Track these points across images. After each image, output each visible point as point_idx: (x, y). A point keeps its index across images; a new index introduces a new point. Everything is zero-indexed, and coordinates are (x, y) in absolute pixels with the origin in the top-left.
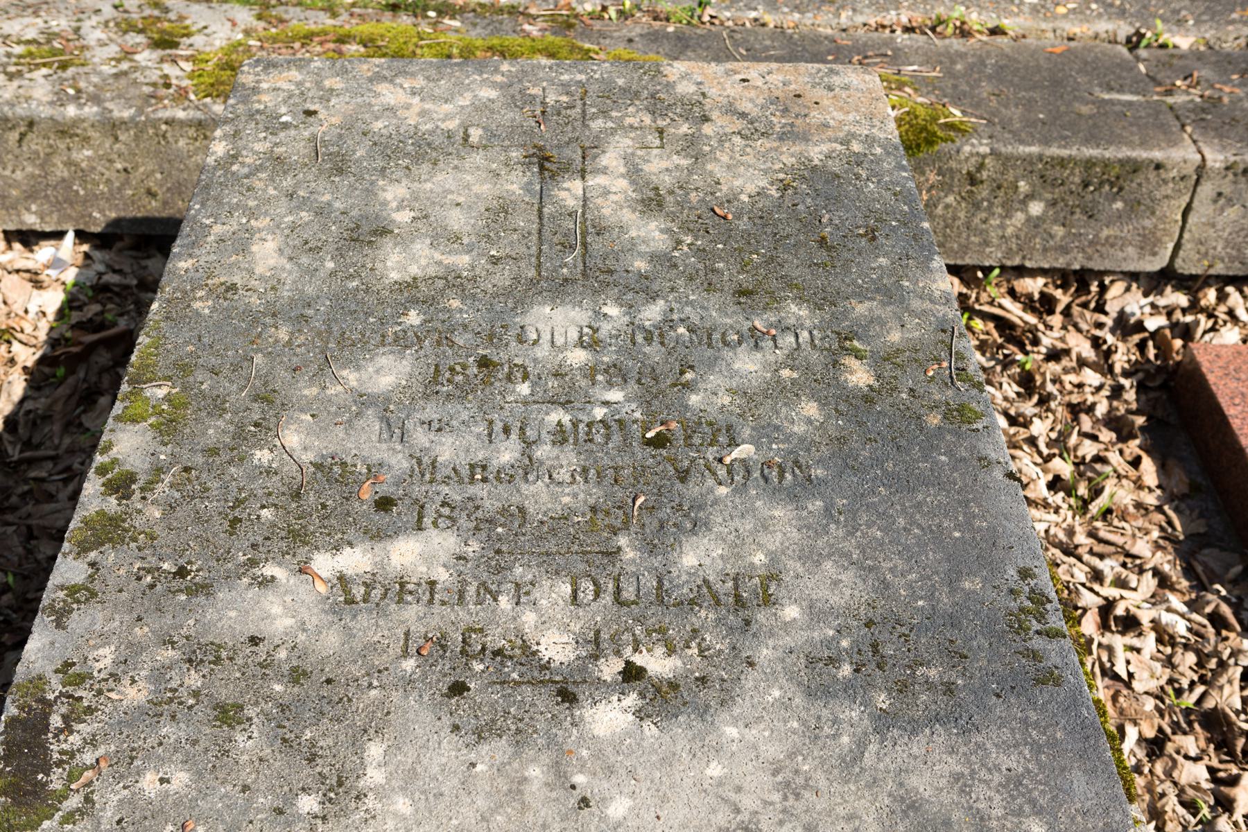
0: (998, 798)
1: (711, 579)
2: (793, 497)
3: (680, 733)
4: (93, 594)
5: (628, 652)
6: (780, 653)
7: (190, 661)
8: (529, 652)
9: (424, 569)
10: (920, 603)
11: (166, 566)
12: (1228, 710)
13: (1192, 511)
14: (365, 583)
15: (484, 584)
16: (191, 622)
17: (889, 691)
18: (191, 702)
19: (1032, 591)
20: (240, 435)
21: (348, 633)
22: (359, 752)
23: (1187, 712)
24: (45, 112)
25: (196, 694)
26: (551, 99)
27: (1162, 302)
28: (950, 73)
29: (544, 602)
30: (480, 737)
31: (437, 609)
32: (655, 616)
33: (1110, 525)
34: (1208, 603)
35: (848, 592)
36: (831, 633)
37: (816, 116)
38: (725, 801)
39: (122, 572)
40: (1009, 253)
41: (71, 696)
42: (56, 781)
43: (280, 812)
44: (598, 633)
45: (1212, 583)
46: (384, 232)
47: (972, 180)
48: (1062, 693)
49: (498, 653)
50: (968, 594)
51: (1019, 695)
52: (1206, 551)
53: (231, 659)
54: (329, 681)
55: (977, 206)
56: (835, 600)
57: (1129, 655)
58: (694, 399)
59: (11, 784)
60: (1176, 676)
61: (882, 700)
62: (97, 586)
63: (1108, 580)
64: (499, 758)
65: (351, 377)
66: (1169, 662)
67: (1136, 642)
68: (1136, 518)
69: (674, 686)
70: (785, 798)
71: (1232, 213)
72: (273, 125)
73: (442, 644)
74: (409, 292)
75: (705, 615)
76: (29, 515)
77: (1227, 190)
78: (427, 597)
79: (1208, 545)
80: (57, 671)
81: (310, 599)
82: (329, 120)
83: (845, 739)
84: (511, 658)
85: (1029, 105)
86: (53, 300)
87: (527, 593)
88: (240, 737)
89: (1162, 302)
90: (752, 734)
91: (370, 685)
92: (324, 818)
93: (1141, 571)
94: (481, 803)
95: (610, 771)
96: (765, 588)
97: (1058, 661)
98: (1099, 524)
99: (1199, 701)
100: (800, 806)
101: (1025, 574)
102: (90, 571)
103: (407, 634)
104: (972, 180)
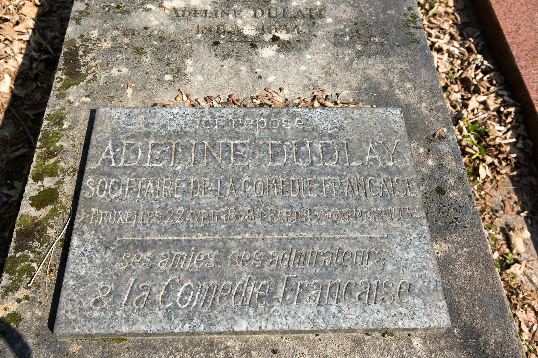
0: (396, 77)
1: (302, 9)
3: (291, 57)
4: (88, 14)
5: (274, 32)
6: (325, 33)
7: (124, 35)
8: (240, 33)
9: (203, 6)
10: (373, 18)
11: (112, 5)
12: (469, 77)
13: (464, 14)
14: (182, 11)
15: (223, 11)
16: (123, 22)
17: (362, 45)
18: (126, 47)
19: (412, 14)
21: (178, 26)
22: (184, 62)
23: (456, 79)
25: (127, 45)
29: (244, 17)
30: (224, 58)
31: (208, 18)
32: (282, 21)
33: (435, 19)
34: (467, 44)
35: (349, 14)
36: (343, 27)
38: (306, 77)
39: (97, 7)
41: (85, 45)
42: (83, 71)
43: (159, 80)
44: (263, 26)
45: (468, 38)
48: (420, 46)
49: (229, 32)
50: (390, 15)
51: (405, 46)
52: (468, 28)
53: (138, 34)
54: (172, 41)
56: (344, 16)
57: (439, 60)
59: (68, 71)
60: (453, 68)
61: (359, 48)
62: (89, 11)
63: (434, 36)
64: (231, 64)
66: (451, 63)
67: (441, 57)
68: (444, 17)
69: (289, 43)
70: (326, 76)
73: (210, 29)
75: (300, 21)
76: (61, 14)
78: (204, 15)
79: (468, 26)
80: (79, 38)
81: (164, 15)
83: (347, 59)
84: (234, 34)
87: (239, 14)
88: (144, 58)
90: (315, 57)
91: (186, 42)
92: (174, 82)
93: (445, 34)
94: (226, 77)
95: (268, 68)
96: (320, 12)
97: (419, 36)
98: (432, 19)
99: (460, 76)
100: (331, 79)
101: (410, 9)
102: (86, 6)
103: (198, 27)
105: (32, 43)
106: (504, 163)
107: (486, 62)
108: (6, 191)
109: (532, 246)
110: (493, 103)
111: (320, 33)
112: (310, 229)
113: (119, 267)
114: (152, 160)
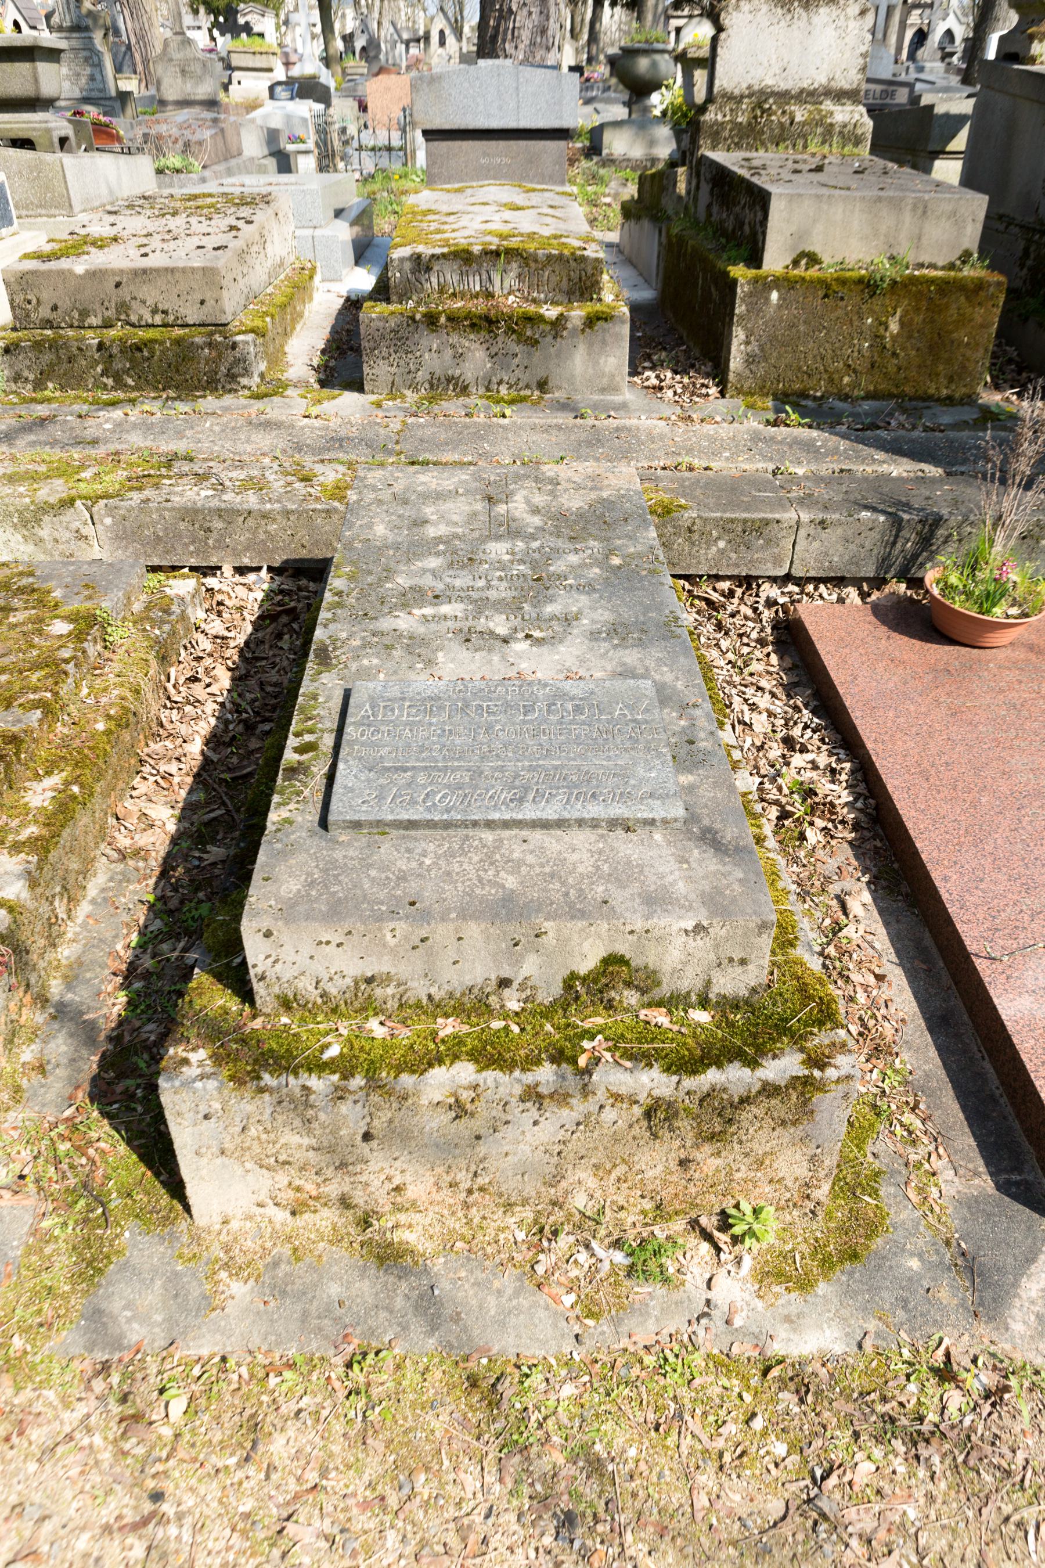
2: (588, 593)
3: (545, 649)
20: (380, 579)
24: (257, 507)
26: (492, 478)
27: (786, 590)
28: (682, 486)
37: (606, 482)
40: (711, 568)
42: (334, 662)
46: (427, 522)
47: (690, 530)
55: (693, 544)
58: (551, 568)
65: (419, 564)
71: (816, 544)
72: (375, 489)
74: (439, 540)
77: (812, 533)
82: (398, 488)
85: (719, 497)
86: (260, 596)
89: (786, 590)
104: (690, 531)
105: (228, 705)
106: (840, 827)
107: (816, 720)
108: (197, 855)
109: (875, 913)
110: (823, 760)
111: (575, 631)
112: (559, 758)
113: (381, 781)
114: (408, 715)
